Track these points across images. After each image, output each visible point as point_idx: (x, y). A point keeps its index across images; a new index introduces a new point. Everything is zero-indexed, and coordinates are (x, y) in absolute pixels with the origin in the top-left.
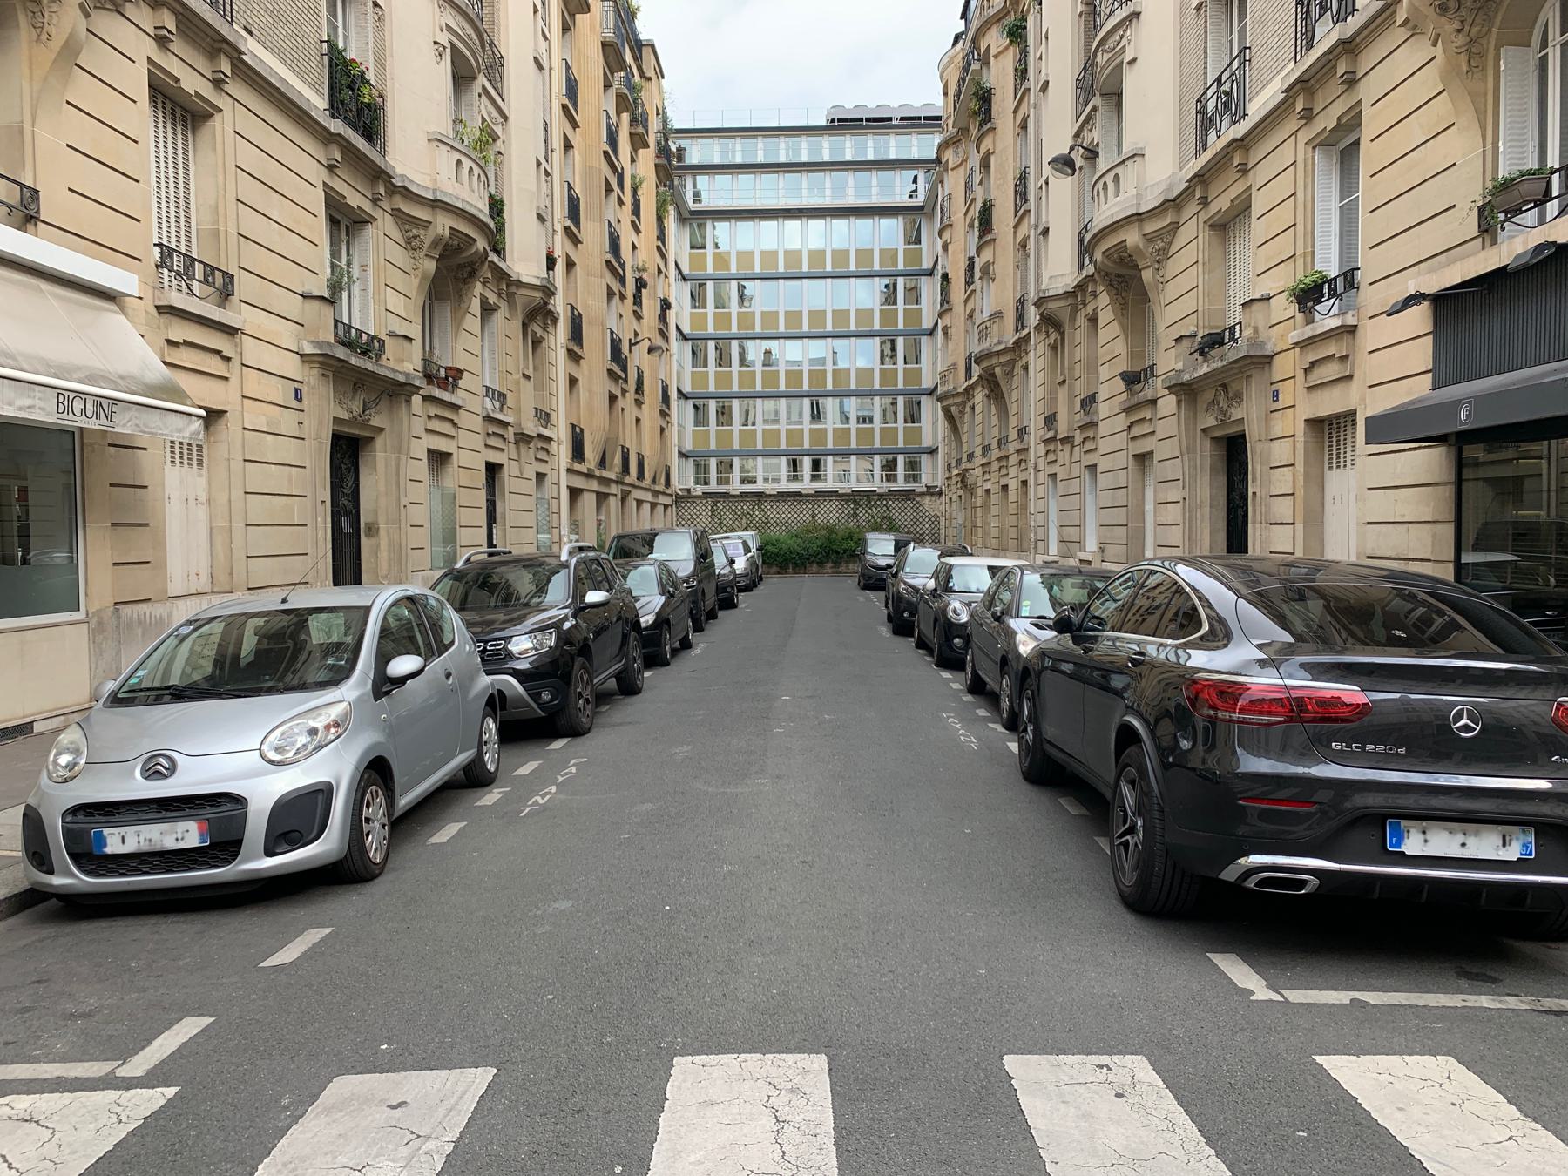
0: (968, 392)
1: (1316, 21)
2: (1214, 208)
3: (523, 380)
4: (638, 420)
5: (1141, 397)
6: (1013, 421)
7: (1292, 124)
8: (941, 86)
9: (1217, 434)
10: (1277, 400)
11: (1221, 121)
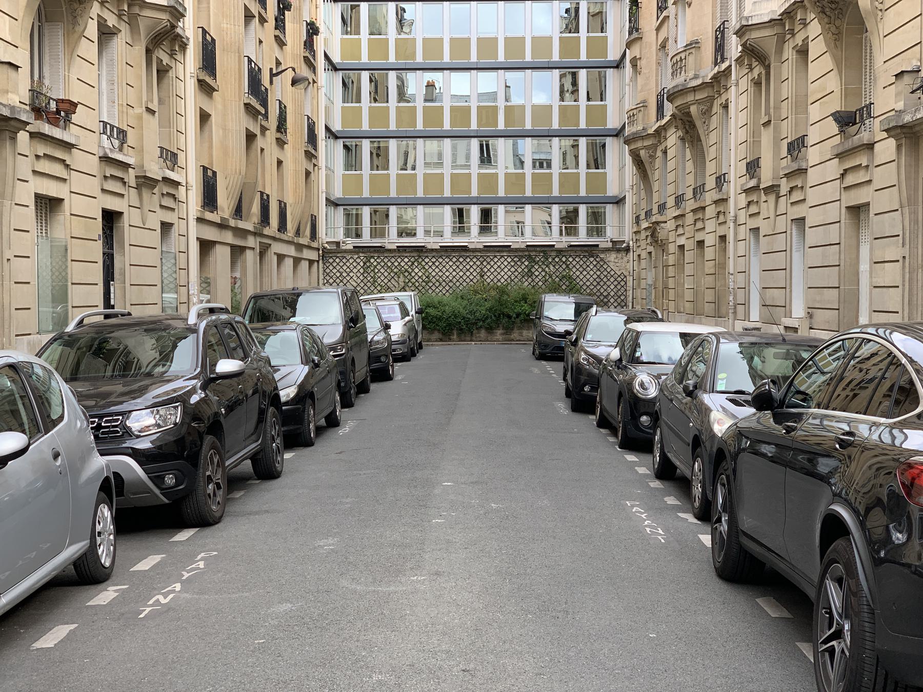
0: (660, 133)
3: (146, 116)
4: (280, 163)
5: (856, 140)
6: (711, 168)
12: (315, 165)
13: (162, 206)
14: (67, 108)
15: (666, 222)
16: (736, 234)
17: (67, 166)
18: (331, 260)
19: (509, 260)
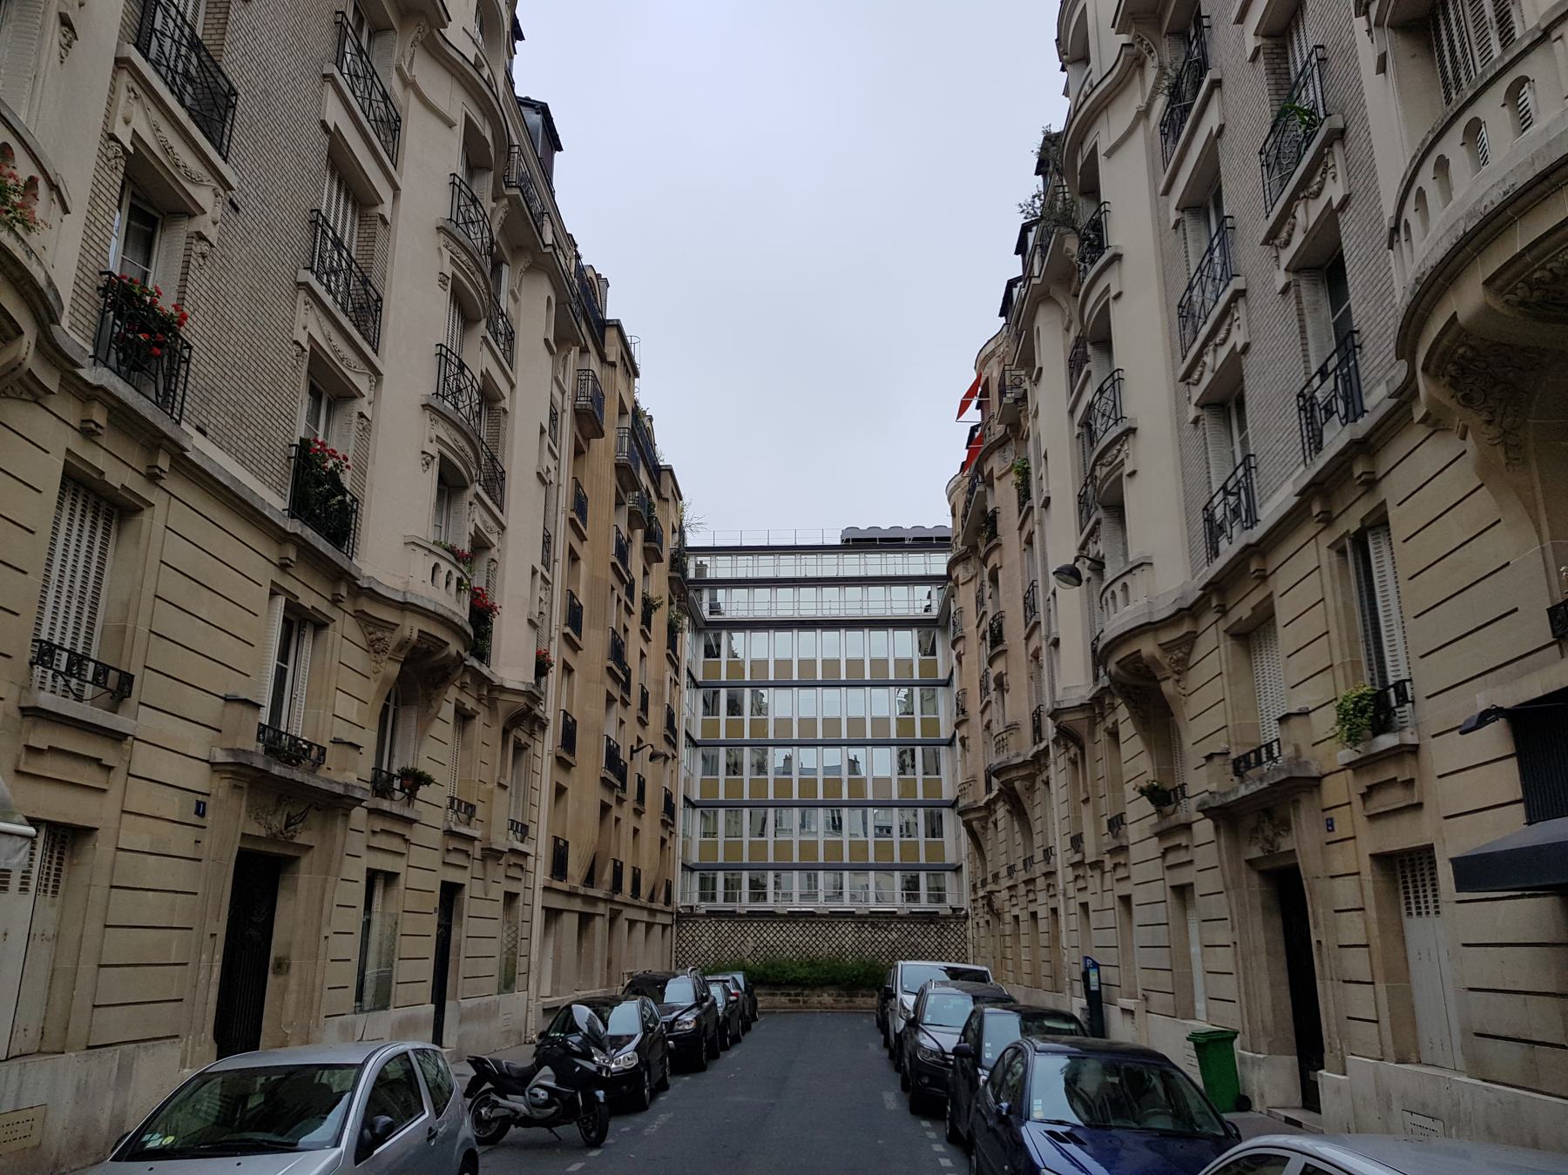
0: (990, 806)
1: (1323, 424)
2: (1234, 616)
3: (497, 790)
4: (636, 831)
5: (1173, 820)
6: (1038, 840)
7: (1310, 529)
8: (949, 508)
9: (1266, 866)
10: (1333, 830)
11: (1232, 528)
12: (671, 833)
13: (507, 877)
14: (415, 780)
15: (1000, 892)
16: (1066, 908)
17: (407, 841)
18: (684, 925)
19: (853, 926)
